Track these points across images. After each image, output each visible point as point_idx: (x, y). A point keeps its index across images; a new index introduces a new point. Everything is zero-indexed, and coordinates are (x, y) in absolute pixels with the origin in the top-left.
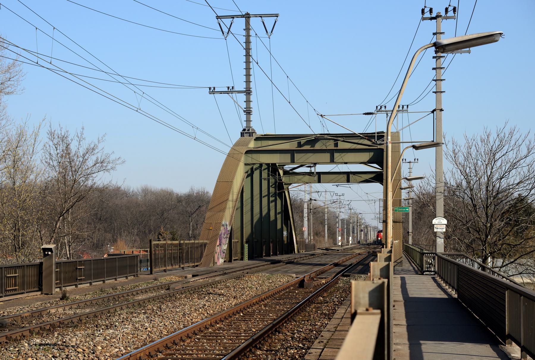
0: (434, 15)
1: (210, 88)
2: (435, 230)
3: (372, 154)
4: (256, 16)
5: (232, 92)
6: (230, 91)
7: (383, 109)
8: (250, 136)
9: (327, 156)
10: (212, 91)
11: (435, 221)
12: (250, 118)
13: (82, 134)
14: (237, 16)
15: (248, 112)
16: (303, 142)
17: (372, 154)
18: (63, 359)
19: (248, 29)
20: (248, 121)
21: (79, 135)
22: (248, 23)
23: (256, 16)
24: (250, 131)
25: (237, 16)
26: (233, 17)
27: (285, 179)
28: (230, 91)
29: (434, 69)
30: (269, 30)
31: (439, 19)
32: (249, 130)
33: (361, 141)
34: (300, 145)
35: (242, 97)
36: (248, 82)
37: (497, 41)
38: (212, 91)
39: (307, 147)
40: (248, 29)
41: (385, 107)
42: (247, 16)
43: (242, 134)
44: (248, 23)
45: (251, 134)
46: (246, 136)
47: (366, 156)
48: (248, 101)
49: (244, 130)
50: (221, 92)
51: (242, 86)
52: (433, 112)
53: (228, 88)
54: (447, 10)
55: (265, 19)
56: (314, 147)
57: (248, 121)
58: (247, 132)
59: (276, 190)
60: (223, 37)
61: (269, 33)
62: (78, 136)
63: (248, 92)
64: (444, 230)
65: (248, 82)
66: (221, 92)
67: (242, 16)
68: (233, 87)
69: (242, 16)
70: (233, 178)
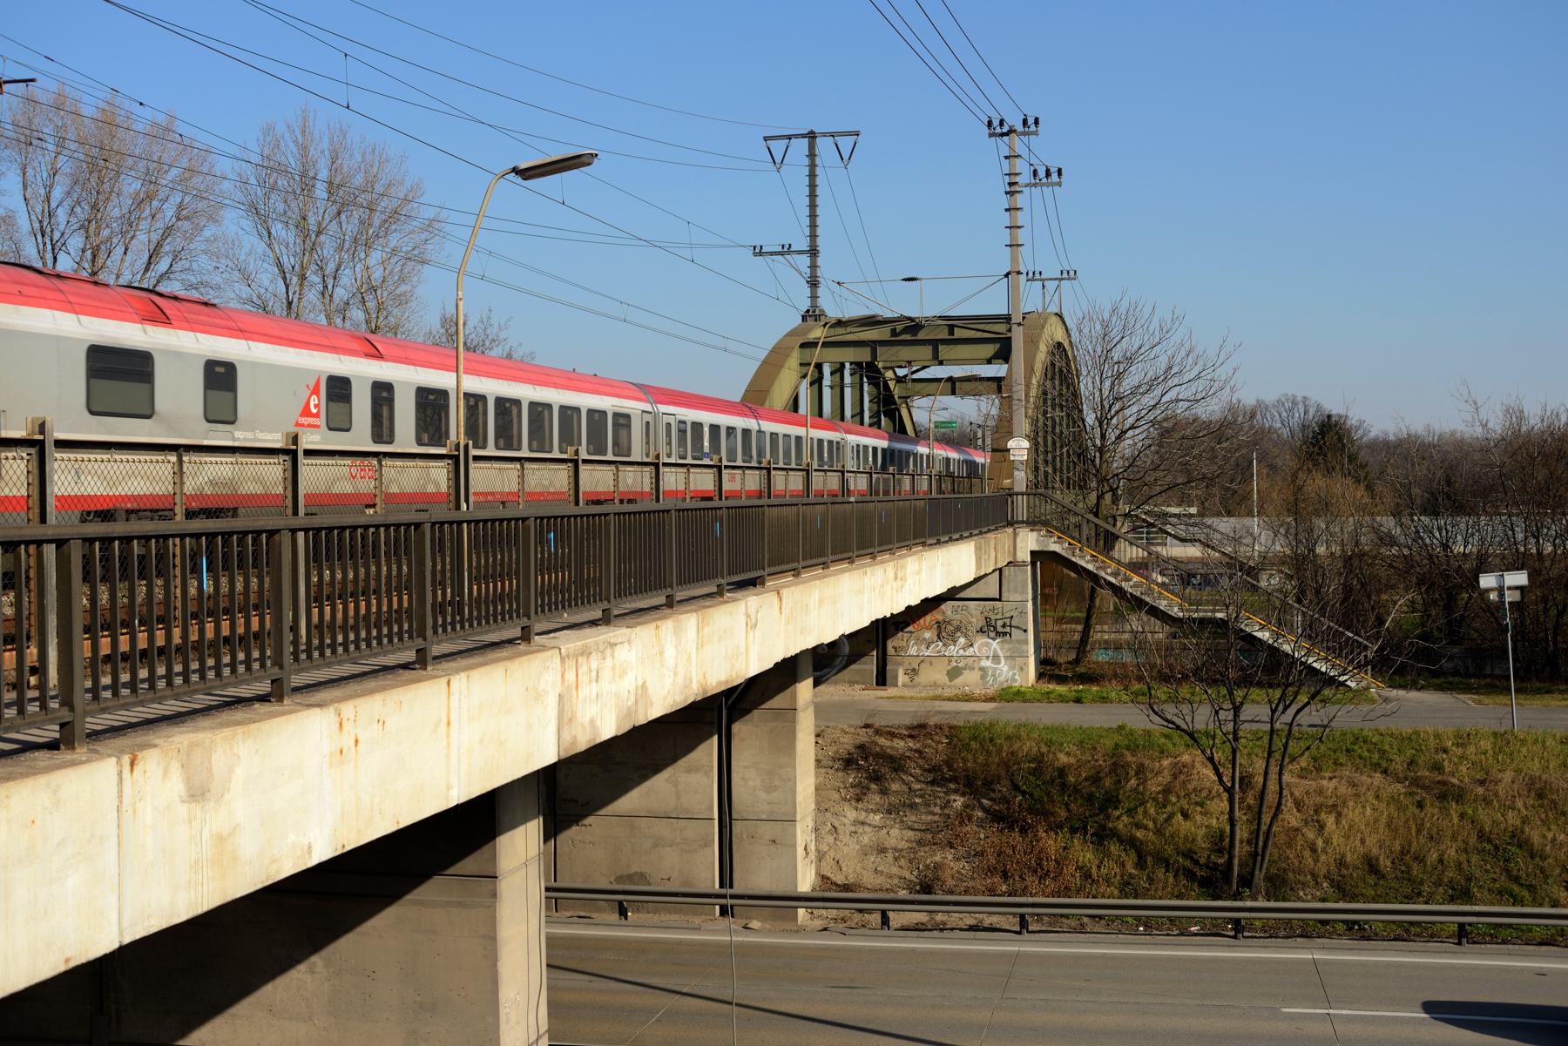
0: (1005, 129)
1: (755, 248)
2: (1012, 458)
3: (997, 346)
4: (824, 135)
5: (789, 252)
6: (786, 251)
7: (1037, 276)
8: (816, 320)
9: (927, 351)
10: (759, 252)
11: (1011, 444)
12: (816, 293)
13: (489, 318)
14: (796, 136)
15: (814, 283)
16: (899, 327)
17: (997, 346)
18: (11, 546)
19: (812, 155)
20: (814, 297)
21: (485, 320)
22: (812, 147)
23: (824, 135)
24: (817, 312)
25: (796, 136)
26: (789, 137)
27: (896, 391)
28: (786, 251)
29: (1006, 210)
30: (846, 157)
31: (1013, 135)
32: (814, 311)
33: (987, 327)
34: (894, 333)
35: (805, 261)
36: (813, 236)
37: (589, 164)
38: (759, 252)
39: (907, 337)
40: (812, 155)
41: (1040, 273)
42: (812, 136)
43: (804, 318)
44: (812, 147)
45: (817, 318)
46: (810, 322)
47: (989, 350)
48: (814, 267)
49: (808, 311)
50: (771, 254)
51: (804, 244)
52: (1007, 275)
53: (783, 246)
54: (1025, 122)
55: (841, 140)
56: (916, 335)
57: (814, 297)
58: (812, 315)
59: (879, 406)
60: (842, 165)
61: (845, 159)
62: (482, 322)
63: (813, 252)
64: (1025, 458)
65: (813, 236)
66: (771, 254)
67: (803, 136)
68: (790, 245)
69: (803, 136)
70: (772, 384)
